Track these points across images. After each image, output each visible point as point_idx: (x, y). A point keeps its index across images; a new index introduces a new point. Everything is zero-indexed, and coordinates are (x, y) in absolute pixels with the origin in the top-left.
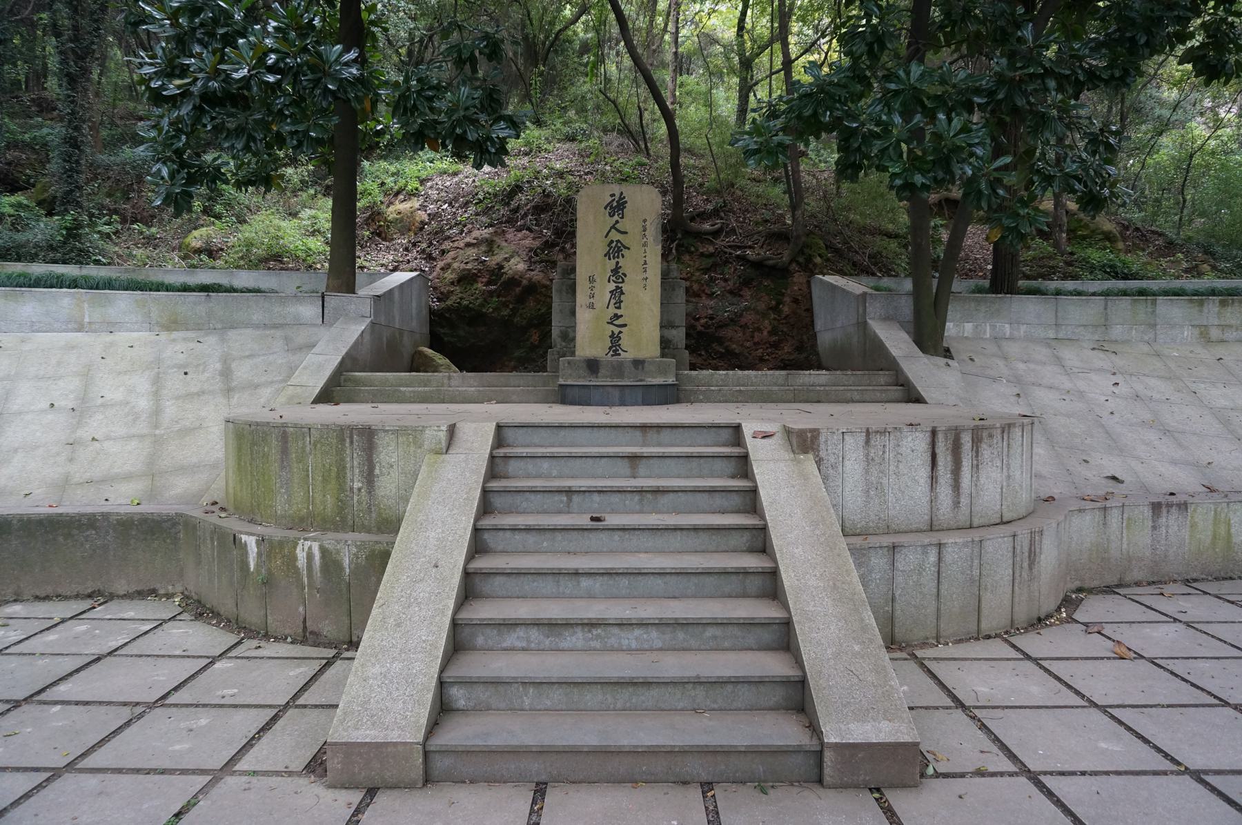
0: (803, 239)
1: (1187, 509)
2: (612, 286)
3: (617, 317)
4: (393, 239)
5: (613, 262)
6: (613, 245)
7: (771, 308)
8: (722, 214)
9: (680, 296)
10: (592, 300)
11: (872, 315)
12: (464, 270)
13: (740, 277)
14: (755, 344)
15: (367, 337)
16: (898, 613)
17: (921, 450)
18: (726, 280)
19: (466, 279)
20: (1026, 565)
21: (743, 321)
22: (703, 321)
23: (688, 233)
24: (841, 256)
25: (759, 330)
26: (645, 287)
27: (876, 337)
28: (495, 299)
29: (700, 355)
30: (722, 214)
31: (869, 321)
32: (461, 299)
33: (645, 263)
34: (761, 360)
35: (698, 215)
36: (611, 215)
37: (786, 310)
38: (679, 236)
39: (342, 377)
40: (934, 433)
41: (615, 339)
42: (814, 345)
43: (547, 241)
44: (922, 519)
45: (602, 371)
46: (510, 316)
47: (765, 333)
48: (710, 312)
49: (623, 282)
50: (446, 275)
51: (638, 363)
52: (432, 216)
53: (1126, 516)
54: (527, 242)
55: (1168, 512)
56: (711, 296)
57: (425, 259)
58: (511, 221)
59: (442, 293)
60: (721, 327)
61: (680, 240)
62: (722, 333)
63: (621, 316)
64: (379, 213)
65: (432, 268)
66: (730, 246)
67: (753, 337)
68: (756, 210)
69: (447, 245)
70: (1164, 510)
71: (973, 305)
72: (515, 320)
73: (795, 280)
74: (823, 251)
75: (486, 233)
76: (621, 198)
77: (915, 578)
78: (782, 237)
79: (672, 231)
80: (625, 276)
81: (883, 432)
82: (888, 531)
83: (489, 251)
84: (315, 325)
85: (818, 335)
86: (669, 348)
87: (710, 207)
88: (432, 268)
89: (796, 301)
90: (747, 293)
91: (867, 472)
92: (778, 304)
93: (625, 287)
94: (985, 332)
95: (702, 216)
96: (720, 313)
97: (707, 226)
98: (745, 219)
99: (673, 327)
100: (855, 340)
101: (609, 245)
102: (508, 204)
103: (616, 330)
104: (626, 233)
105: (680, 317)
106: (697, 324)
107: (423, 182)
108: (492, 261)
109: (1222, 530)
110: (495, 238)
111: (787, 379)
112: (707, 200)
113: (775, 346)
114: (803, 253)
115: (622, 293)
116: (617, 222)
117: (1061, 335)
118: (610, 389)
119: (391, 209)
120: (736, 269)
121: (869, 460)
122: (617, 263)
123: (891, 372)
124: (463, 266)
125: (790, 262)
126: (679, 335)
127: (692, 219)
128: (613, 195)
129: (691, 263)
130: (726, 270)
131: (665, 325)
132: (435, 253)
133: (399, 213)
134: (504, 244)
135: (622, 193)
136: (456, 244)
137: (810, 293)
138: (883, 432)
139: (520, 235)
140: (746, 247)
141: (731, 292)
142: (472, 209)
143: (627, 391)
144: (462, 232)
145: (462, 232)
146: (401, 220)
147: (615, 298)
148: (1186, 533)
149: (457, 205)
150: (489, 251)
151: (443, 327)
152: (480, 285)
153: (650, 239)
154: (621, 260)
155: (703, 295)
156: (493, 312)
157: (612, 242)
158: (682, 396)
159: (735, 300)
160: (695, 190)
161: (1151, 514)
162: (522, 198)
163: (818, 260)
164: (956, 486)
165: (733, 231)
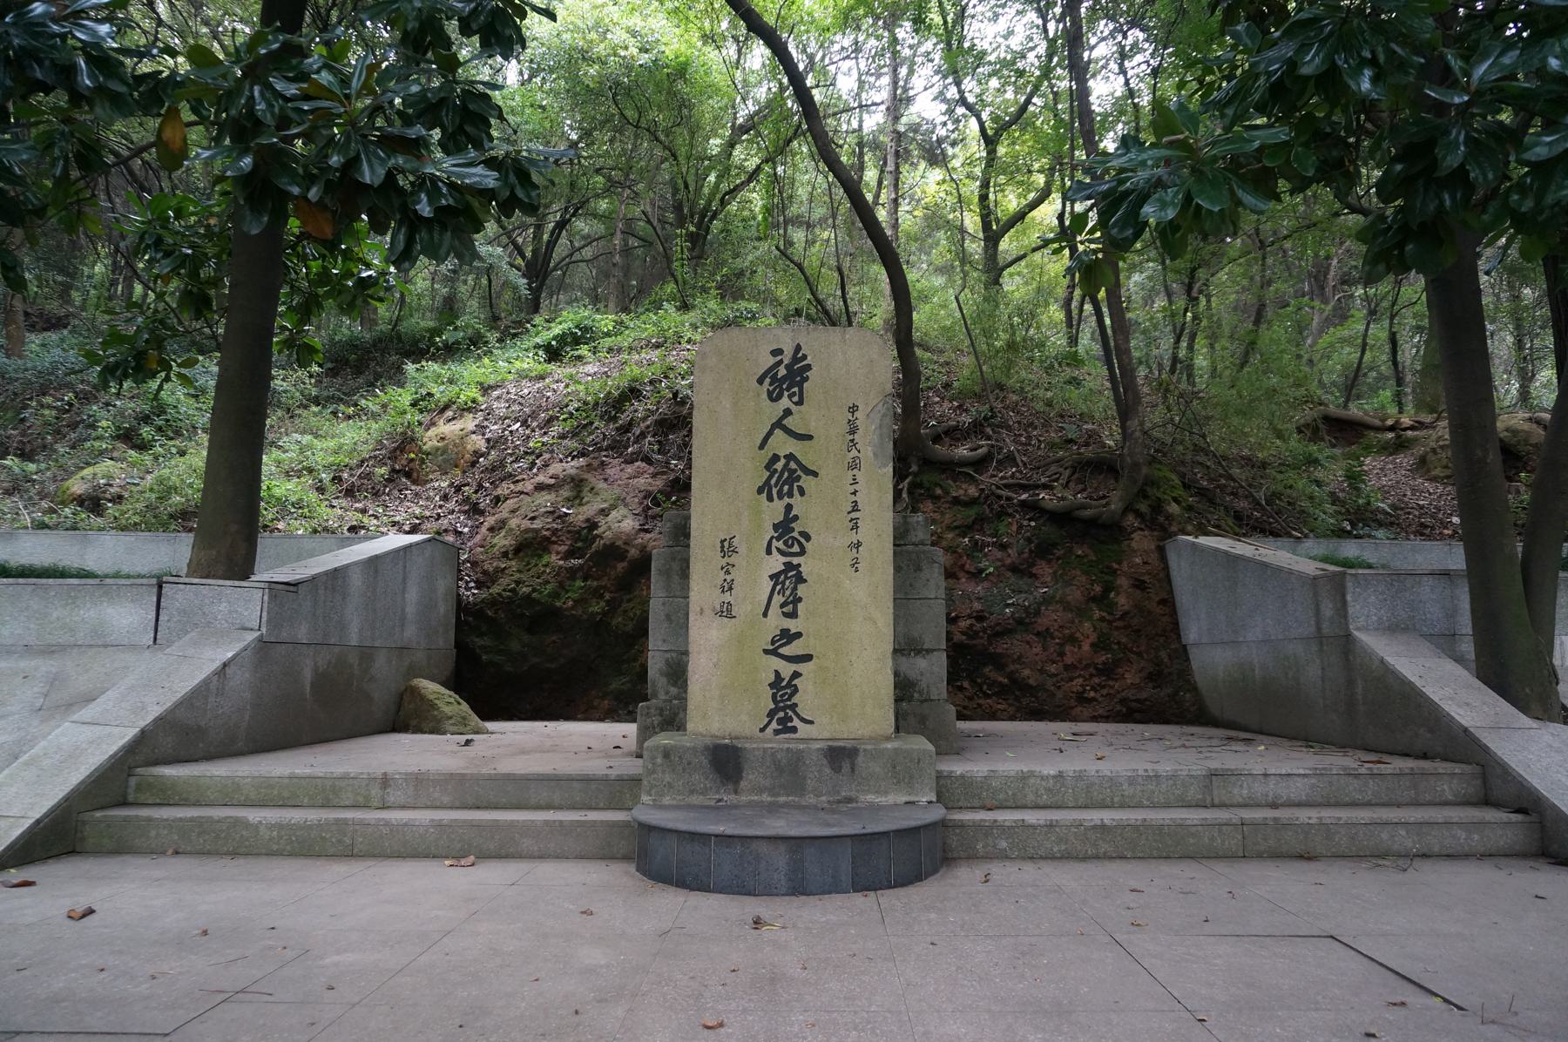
0: (1145, 470)
2: (776, 563)
3: (788, 636)
4: (427, 482)
5: (779, 506)
6: (779, 466)
7: (1093, 599)
8: (989, 431)
9: (933, 584)
10: (727, 597)
11: (1362, 622)
12: (527, 530)
13: (1029, 540)
14: (1067, 667)
15: (240, 678)
18: (1003, 547)
19: (530, 546)
21: (1043, 622)
22: (963, 624)
23: (929, 463)
24: (1212, 502)
25: (1072, 639)
26: (855, 565)
27: (1388, 671)
28: (579, 583)
30: (989, 431)
31: (1356, 633)
32: (518, 582)
33: (855, 508)
34: (1082, 699)
35: (947, 433)
36: (774, 398)
37: (1122, 601)
38: (914, 468)
39: (133, 781)
41: (783, 692)
42: (1185, 672)
45: (750, 777)
46: (604, 614)
47: (1086, 647)
48: (977, 606)
49: (802, 552)
50: (495, 541)
51: (840, 756)
52: (492, 443)
54: (642, 482)
56: (976, 575)
57: (465, 512)
58: (616, 447)
59: (485, 573)
60: (997, 635)
61: (916, 475)
62: (1002, 646)
63: (799, 635)
64: (413, 440)
65: (475, 529)
66: (1006, 486)
67: (1062, 654)
68: (1046, 425)
69: (504, 489)
72: (614, 622)
73: (1134, 544)
74: (1180, 492)
75: (572, 467)
78: (1103, 467)
80: (808, 538)
83: (575, 498)
84: (133, 647)
85: (1194, 654)
86: (910, 699)
87: (966, 419)
88: (475, 529)
89: (1140, 585)
90: (1044, 570)
92: (1107, 589)
93: (807, 565)
95: (954, 434)
96: (996, 609)
97: (963, 451)
98: (1029, 438)
99: (919, 652)
100: (1312, 672)
101: (768, 467)
102: (614, 419)
103: (787, 669)
104: (810, 437)
105: (934, 631)
107: (486, 389)
108: (579, 515)
110: (586, 476)
112: (960, 407)
113: (1108, 671)
114: (1146, 497)
115: (800, 579)
116: (788, 412)
118: (763, 848)
119: (432, 432)
120: (1021, 527)
122: (789, 508)
123: (1467, 768)
124: (526, 524)
125: (1125, 511)
126: (933, 669)
127: (937, 439)
128: (777, 352)
130: (1002, 529)
131: (905, 647)
132: (485, 503)
133: (443, 439)
134: (602, 485)
135: (798, 348)
136: (519, 487)
137: (1166, 568)
139: (630, 469)
140: (1037, 487)
141: (1014, 569)
142: (556, 429)
144: (533, 464)
145: (533, 464)
146: (444, 451)
149: (535, 424)
150: (575, 498)
151: (481, 635)
152: (554, 557)
153: (867, 452)
154: (796, 500)
155: (961, 574)
156: (573, 608)
157: (776, 458)
159: (1023, 583)
160: (938, 395)
162: (639, 408)
163: (1174, 508)
165: (1010, 459)
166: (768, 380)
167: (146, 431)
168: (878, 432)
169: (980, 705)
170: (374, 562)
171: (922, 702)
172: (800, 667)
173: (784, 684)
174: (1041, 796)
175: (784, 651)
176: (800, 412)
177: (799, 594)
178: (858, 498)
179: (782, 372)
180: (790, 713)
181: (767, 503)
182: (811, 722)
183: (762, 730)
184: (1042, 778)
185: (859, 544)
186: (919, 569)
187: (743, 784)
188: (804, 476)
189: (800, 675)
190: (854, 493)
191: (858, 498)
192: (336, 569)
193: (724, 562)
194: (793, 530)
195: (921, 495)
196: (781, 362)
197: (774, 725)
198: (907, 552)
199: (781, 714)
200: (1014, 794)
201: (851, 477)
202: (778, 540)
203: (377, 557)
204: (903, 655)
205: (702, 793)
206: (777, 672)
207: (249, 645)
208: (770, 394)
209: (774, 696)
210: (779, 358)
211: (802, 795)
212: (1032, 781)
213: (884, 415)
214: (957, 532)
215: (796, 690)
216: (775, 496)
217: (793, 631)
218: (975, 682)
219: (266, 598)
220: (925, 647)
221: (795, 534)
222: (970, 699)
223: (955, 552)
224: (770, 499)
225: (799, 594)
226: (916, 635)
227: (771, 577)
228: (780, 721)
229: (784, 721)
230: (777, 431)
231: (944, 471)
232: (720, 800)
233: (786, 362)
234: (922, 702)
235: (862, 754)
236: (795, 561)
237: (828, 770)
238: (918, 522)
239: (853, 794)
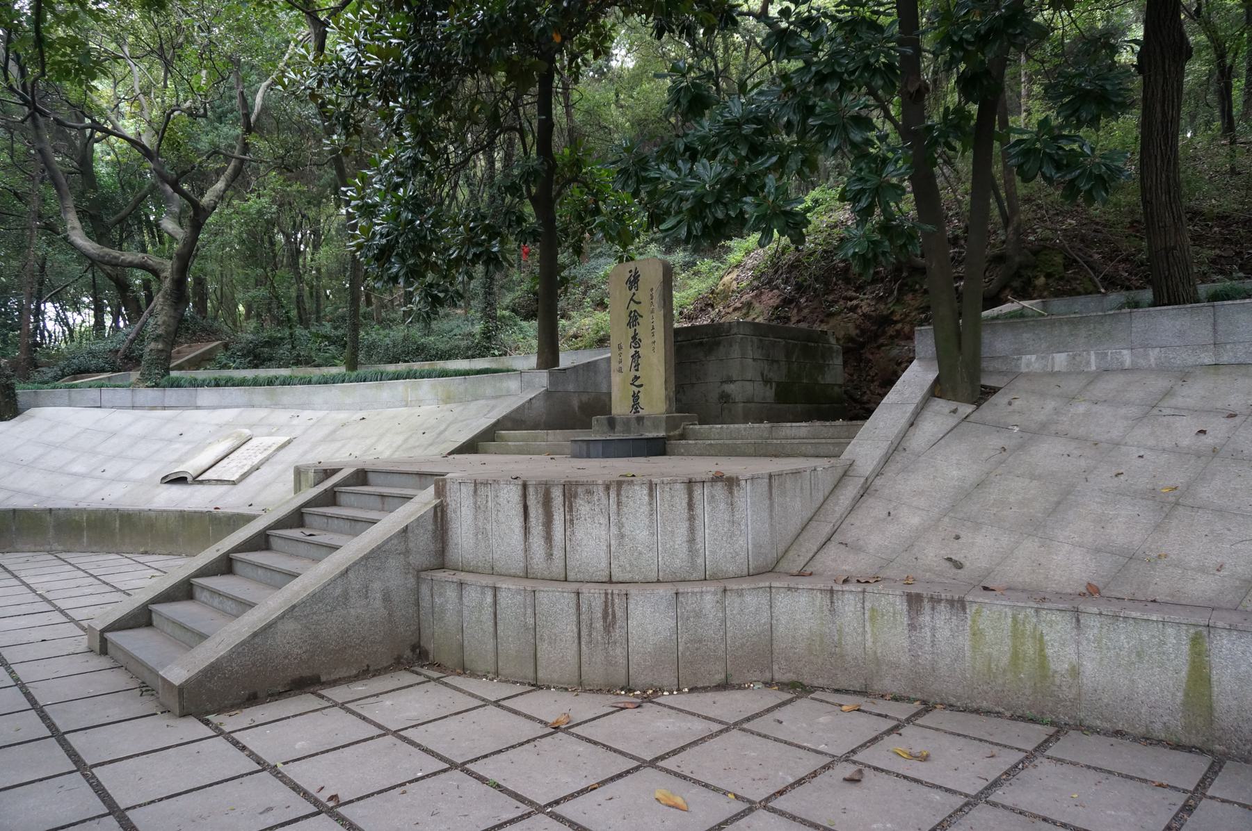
1: (964, 609)
2: (632, 351)
3: (636, 378)
5: (633, 329)
16: (466, 643)
17: (515, 501)
20: (599, 625)
40: (525, 486)
44: (517, 566)
45: (618, 428)
53: (868, 605)
55: (933, 609)
61: (904, 278)
70: (927, 605)
71: (1066, 328)
76: (636, 273)
77: (477, 614)
81: (485, 484)
82: (493, 572)
91: (476, 519)
94: (1088, 363)
109: (1030, 648)
111: (771, 432)
117: (1225, 359)
121: (477, 508)
128: (631, 271)
134: (758, 305)
138: (485, 484)
143: (591, 445)
148: (965, 641)
154: (637, 327)
158: (668, 450)
161: (905, 607)
164: (548, 538)
172: (641, 389)
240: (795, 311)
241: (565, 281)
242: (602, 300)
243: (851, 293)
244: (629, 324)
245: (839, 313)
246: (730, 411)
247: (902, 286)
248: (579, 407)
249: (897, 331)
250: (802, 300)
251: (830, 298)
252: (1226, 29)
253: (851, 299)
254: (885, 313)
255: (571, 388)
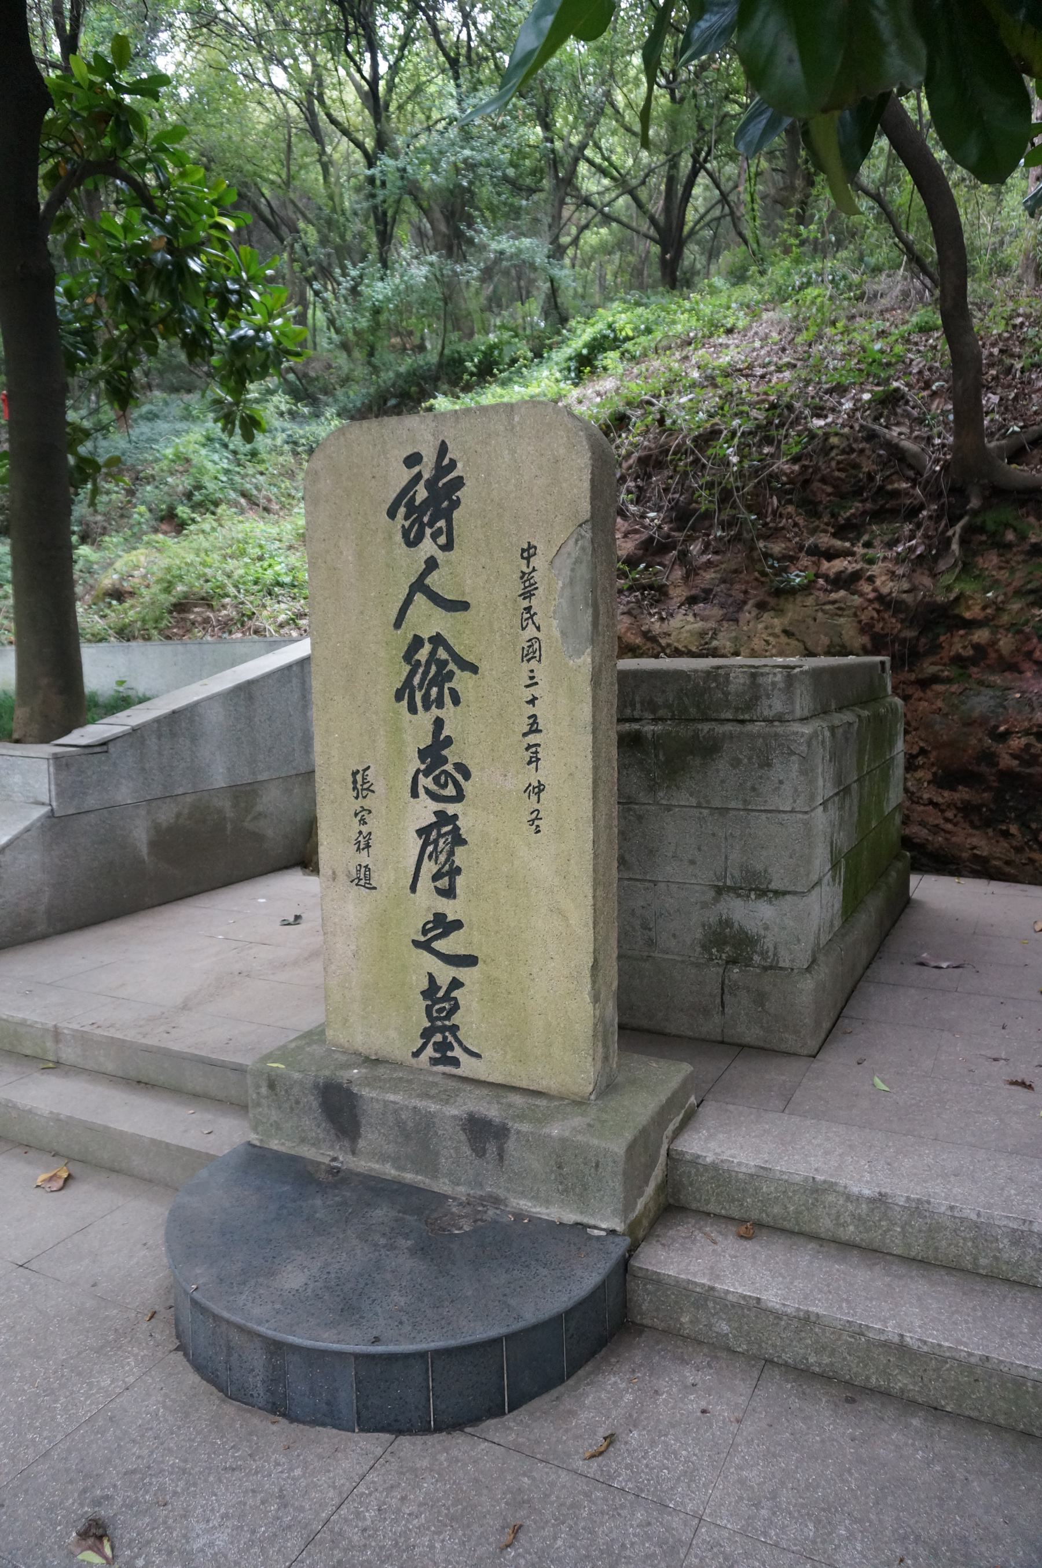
2: (425, 811)
5: (425, 719)
6: (423, 655)
10: (364, 858)
22: (1017, 743)
26: (535, 819)
29: (1006, 834)
33: (534, 728)
36: (412, 541)
43: (651, 539)
45: (370, 1137)
49: (459, 797)
61: (975, 513)
63: (458, 925)
79: (953, 490)
80: (467, 775)
99: (765, 893)
103: (445, 974)
104: (464, 606)
106: (1000, 748)
115: (459, 840)
116: (432, 564)
122: (439, 723)
128: (413, 460)
129: (1003, 575)
135: (443, 449)
147: (434, 856)
154: (448, 712)
155: (1026, 665)
157: (417, 642)
166: (402, 510)
167: (183, 511)
168: (567, 592)
169: (1032, 861)
170: (246, 690)
171: (765, 969)
172: (463, 973)
173: (441, 994)
174: (845, 1225)
175: (439, 945)
176: (448, 562)
177: (457, 863)
178: (538, 710)
179: (422, 494)
180: (450, 1039)
181: (408, 716)
182: (478, 1056)
183: (416, 1054)
184: (848, 1197)
185: (540, 788)
186: (767, 764)
187: (361, 1143)
188: (457, 672)
189: (461, 985)
190: (532, 701)
191: (538, 710)
192: (174, 712)
193: (357, 805)
194: (445, 760)
195: (981, 543)
196: (418, 476)
197: (429, 1051)
198: (751, 736)
199: (438, 1037)
200: (798, 1213)
201: (526, 674)
202: (426, 776)
203: (250, 683)
204: (739, 896)
205: (313, 1145)
206: (431, 977)
207: (32, 825)
208: (406, 533)
209: (428, 1010)
210: (416, 470)
211: (434, 1177)
212: (831, 1198)
213: (578, 561)
214: (1031, 598)
215: (456, 1007)
216: (419, 704)
217: (451, 918)
218: (1029, 827)
219: (52, 769)
220: (773, 886)
221: (449, 767)
222: (1019, 850)
223: (1019, 632)
224: (413, 709)
225: (458, 863)
226: (759, 867)
227: (420, 832)
228: (437, 1047)
229: (443, 1047)
230: (419, 598)
231: (1023, 504)
232: (335, 1159)
233: (426, 476)
234: (765, 969)
235: (513, 1137)
236: (451, 809)
237: (466, 1150)
238: (774, 684)
239: (501, 1193)
240: (678, 573)
241: (88, 469)
242: (171, 509)
243: (825, 540)
244: (404, 692)
245: (807, 588)
246: (760, 998)
247: (969, 531)
248: (153, 844)
249: (977, 647)
250: (695, 548)
251: (777, 548)
252: (271, 392)
253: (830, 555)
254: (940, 599)
255: (124, 793)
